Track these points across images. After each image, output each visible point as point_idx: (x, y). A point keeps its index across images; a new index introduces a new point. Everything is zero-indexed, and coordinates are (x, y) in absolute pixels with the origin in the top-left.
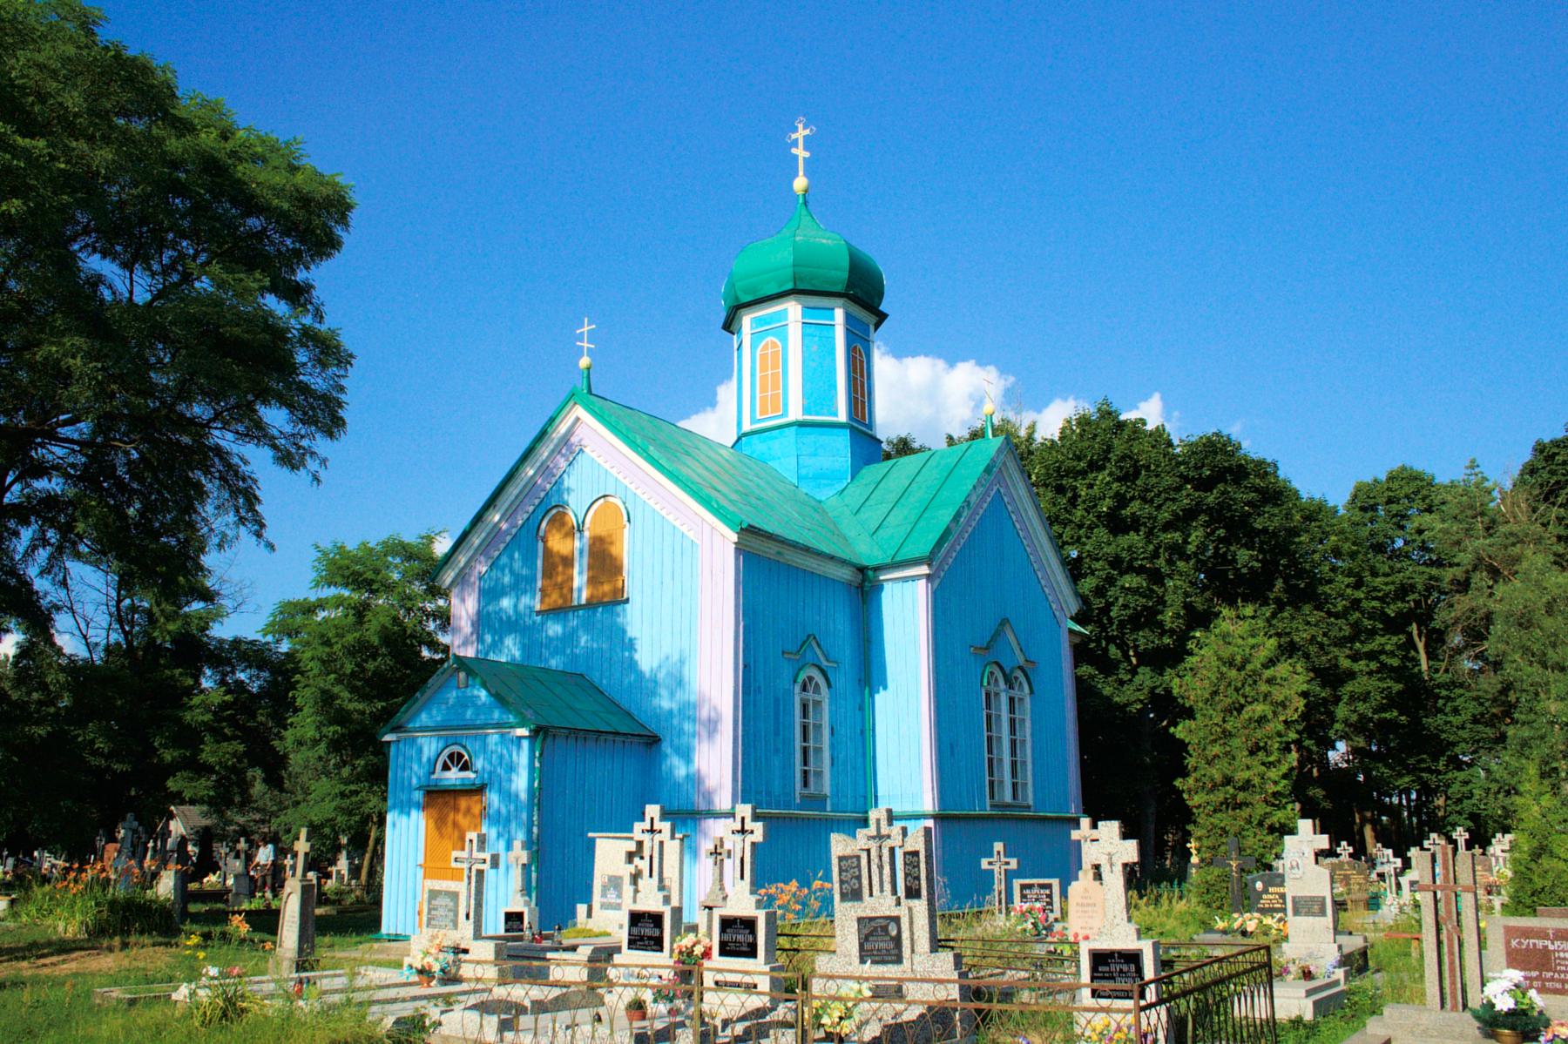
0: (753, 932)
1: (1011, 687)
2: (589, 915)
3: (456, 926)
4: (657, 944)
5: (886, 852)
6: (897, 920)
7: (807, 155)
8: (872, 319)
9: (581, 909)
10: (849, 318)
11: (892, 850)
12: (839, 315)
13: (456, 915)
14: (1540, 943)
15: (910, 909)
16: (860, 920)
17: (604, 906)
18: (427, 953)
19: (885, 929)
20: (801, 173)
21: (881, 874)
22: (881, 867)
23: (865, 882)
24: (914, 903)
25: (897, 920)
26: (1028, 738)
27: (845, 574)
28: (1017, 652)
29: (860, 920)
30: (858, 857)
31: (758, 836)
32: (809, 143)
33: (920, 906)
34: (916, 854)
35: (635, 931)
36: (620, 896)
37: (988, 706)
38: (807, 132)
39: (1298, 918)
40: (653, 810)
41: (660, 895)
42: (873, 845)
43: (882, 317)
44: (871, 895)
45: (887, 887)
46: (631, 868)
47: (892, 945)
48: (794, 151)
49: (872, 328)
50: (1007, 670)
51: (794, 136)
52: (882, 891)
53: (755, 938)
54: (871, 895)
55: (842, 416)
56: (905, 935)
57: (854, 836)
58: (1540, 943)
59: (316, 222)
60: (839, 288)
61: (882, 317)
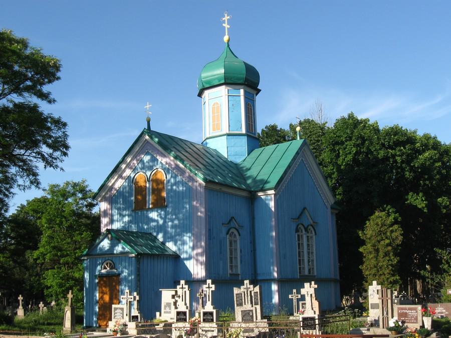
0: (212, 316)
1: (308, 233)
2: (160, 315)
3: (123, 318)
4: (185, 320)
5: (249, 292)
6: (252, 311)
7: (229, 27)
8: (255, 92)
9: (158, 314)
10: (245, 92)
11: (251, 292)
12: (242, 91)
13: (123, 315)
14: (405, 311)
15: (256, 308)
16: (242, 311)
17: (165, 312)
18: (115, 326)
19: (249, 313)
20: (227, 34)
21: (248, 299)
22: (248, 296)
23: (243, 301)
24: (257, 306)
25: (252, 311)
26: (314, 251)
27: (244, 194)
28: (310, 218)
29: (242, 311)
30: (242, 294)
31: (213, 289)
32: (229, 22)
33: (258, 307)
34: (257, 292)
35: (178, 317)
36: (170, 309)
37: (299, 240)
38: (229, 17)
39: (372, 310)
40: (182, 282)
41: (185, 307)
42: (246, 291)
43: (259, 91)
44: (245, 304)
45: (249, 302)
46: (174, 300)
47: (251, 318)
48: (224, 25)
49: (255, 95)
50: (306, 226)
51: (224, 19)
52: (248, 303)
53: (213, 317)
54: (245, 304)
55: (244, 131)
56: (254, 315)
57: (240, 288)
58: (405, 311)
59: (47, 71)
60: (241, 81)
61: (259, 91)
